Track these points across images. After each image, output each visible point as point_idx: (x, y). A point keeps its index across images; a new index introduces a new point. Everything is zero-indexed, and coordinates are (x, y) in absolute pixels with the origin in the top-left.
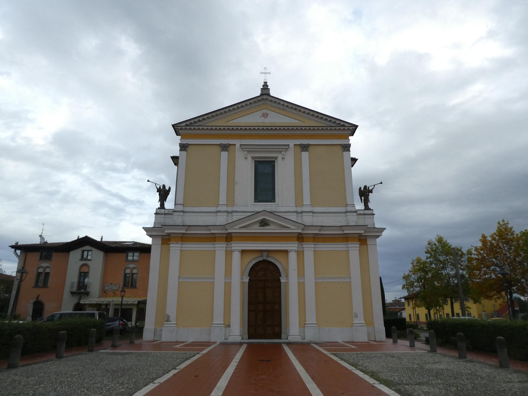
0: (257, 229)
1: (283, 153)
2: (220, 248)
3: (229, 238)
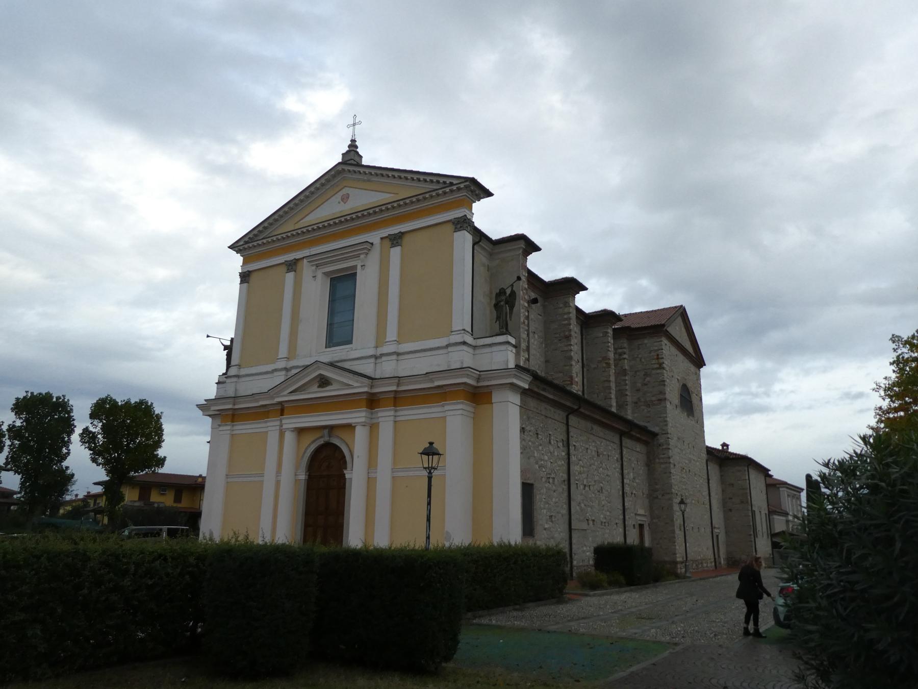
0: (315, 392)
1: (362, 256)
2: (271, 427)
3: (282, 410)
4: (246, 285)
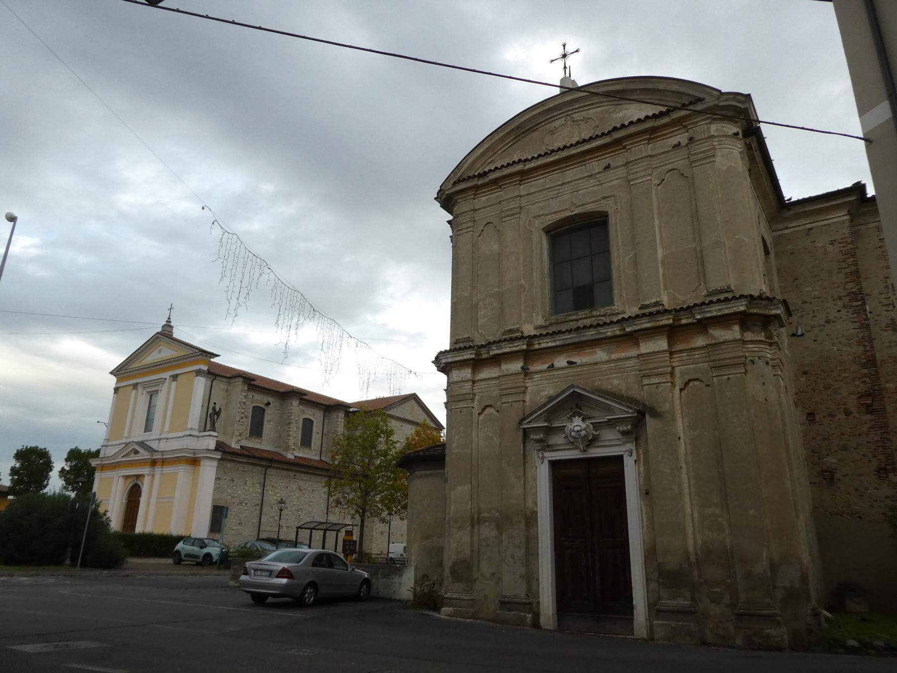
0: (133, 457)
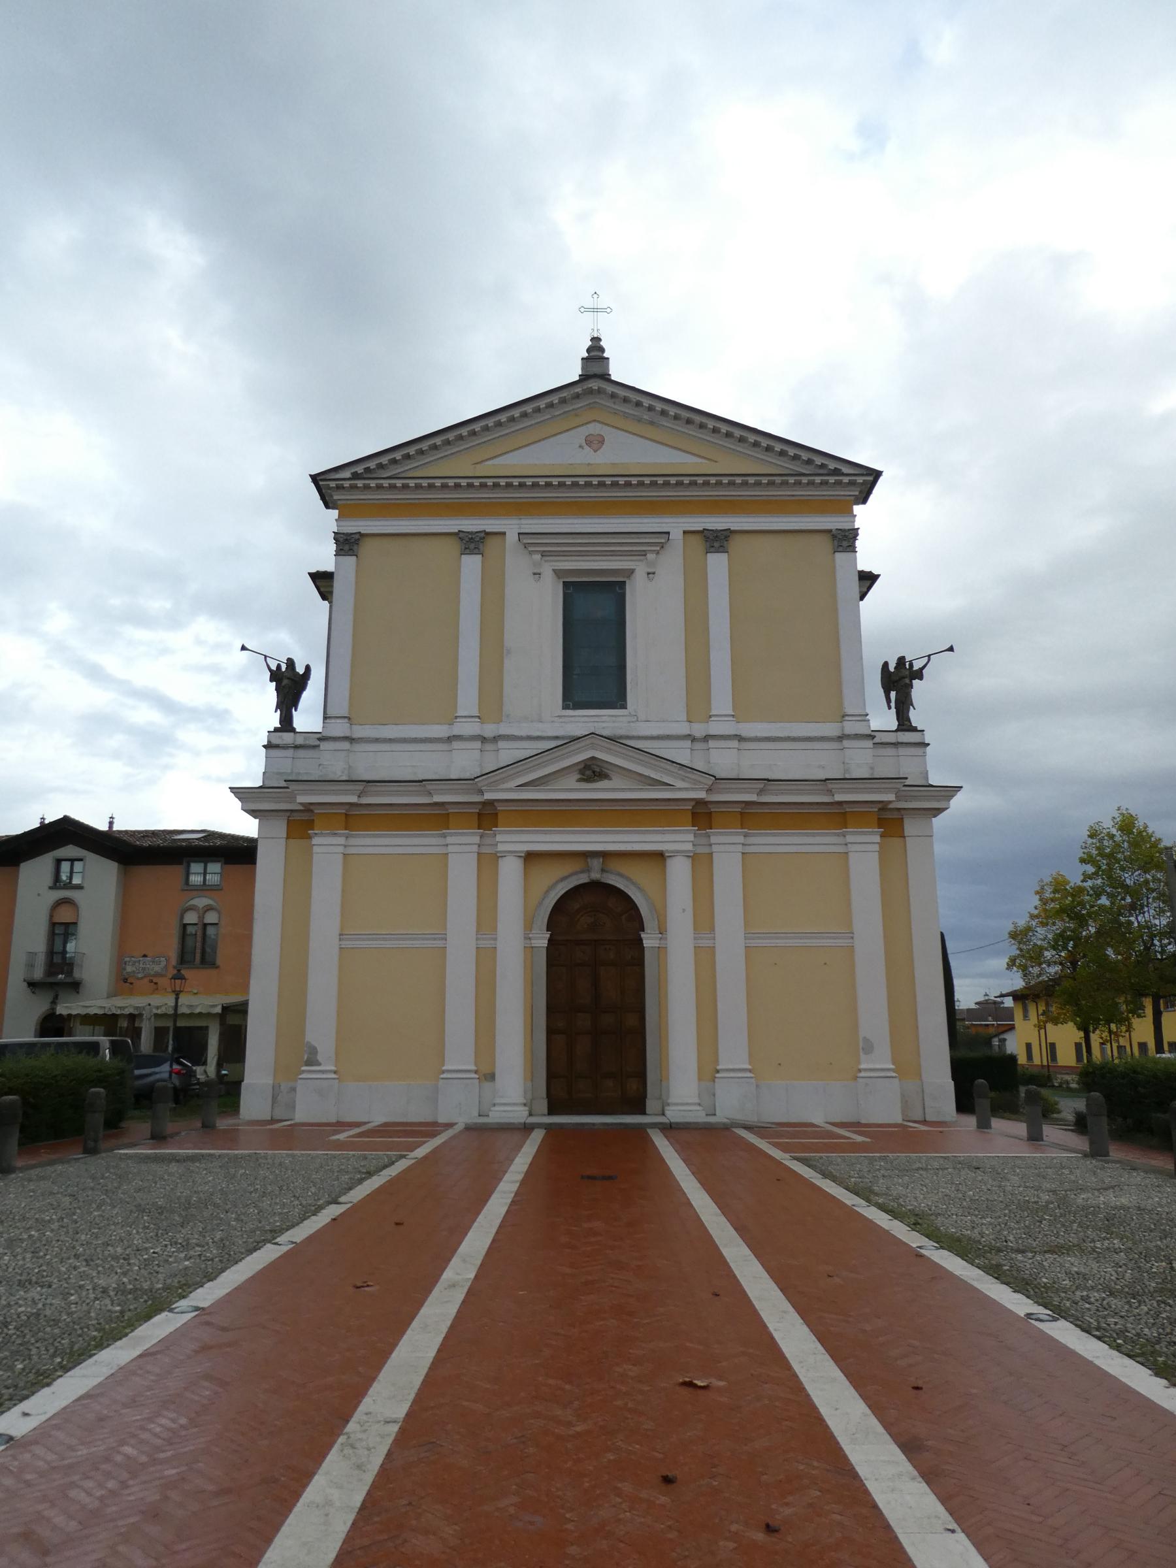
0: (572, 790)
1: (651, 556)
2: (461, 848)
3: (487, 816)
4: (351, 560)
